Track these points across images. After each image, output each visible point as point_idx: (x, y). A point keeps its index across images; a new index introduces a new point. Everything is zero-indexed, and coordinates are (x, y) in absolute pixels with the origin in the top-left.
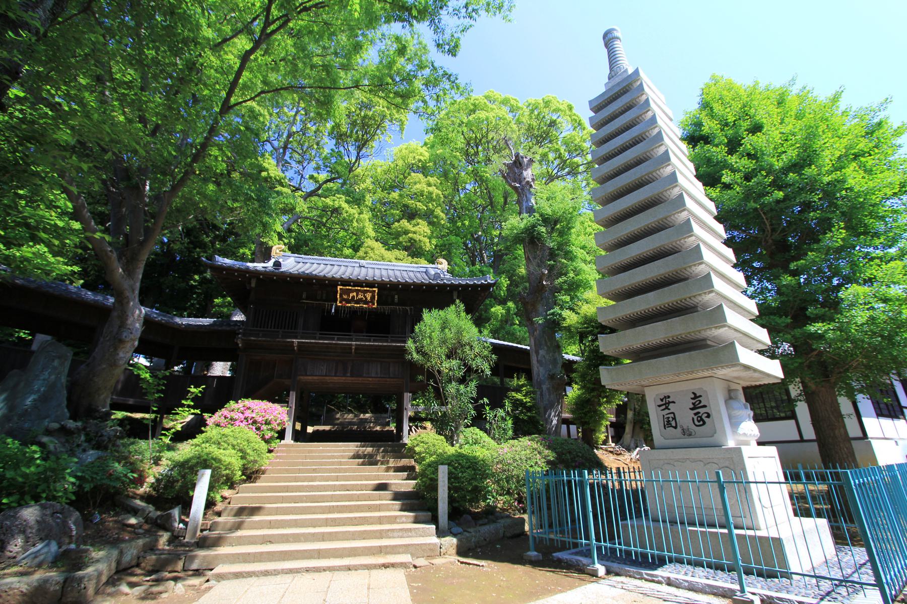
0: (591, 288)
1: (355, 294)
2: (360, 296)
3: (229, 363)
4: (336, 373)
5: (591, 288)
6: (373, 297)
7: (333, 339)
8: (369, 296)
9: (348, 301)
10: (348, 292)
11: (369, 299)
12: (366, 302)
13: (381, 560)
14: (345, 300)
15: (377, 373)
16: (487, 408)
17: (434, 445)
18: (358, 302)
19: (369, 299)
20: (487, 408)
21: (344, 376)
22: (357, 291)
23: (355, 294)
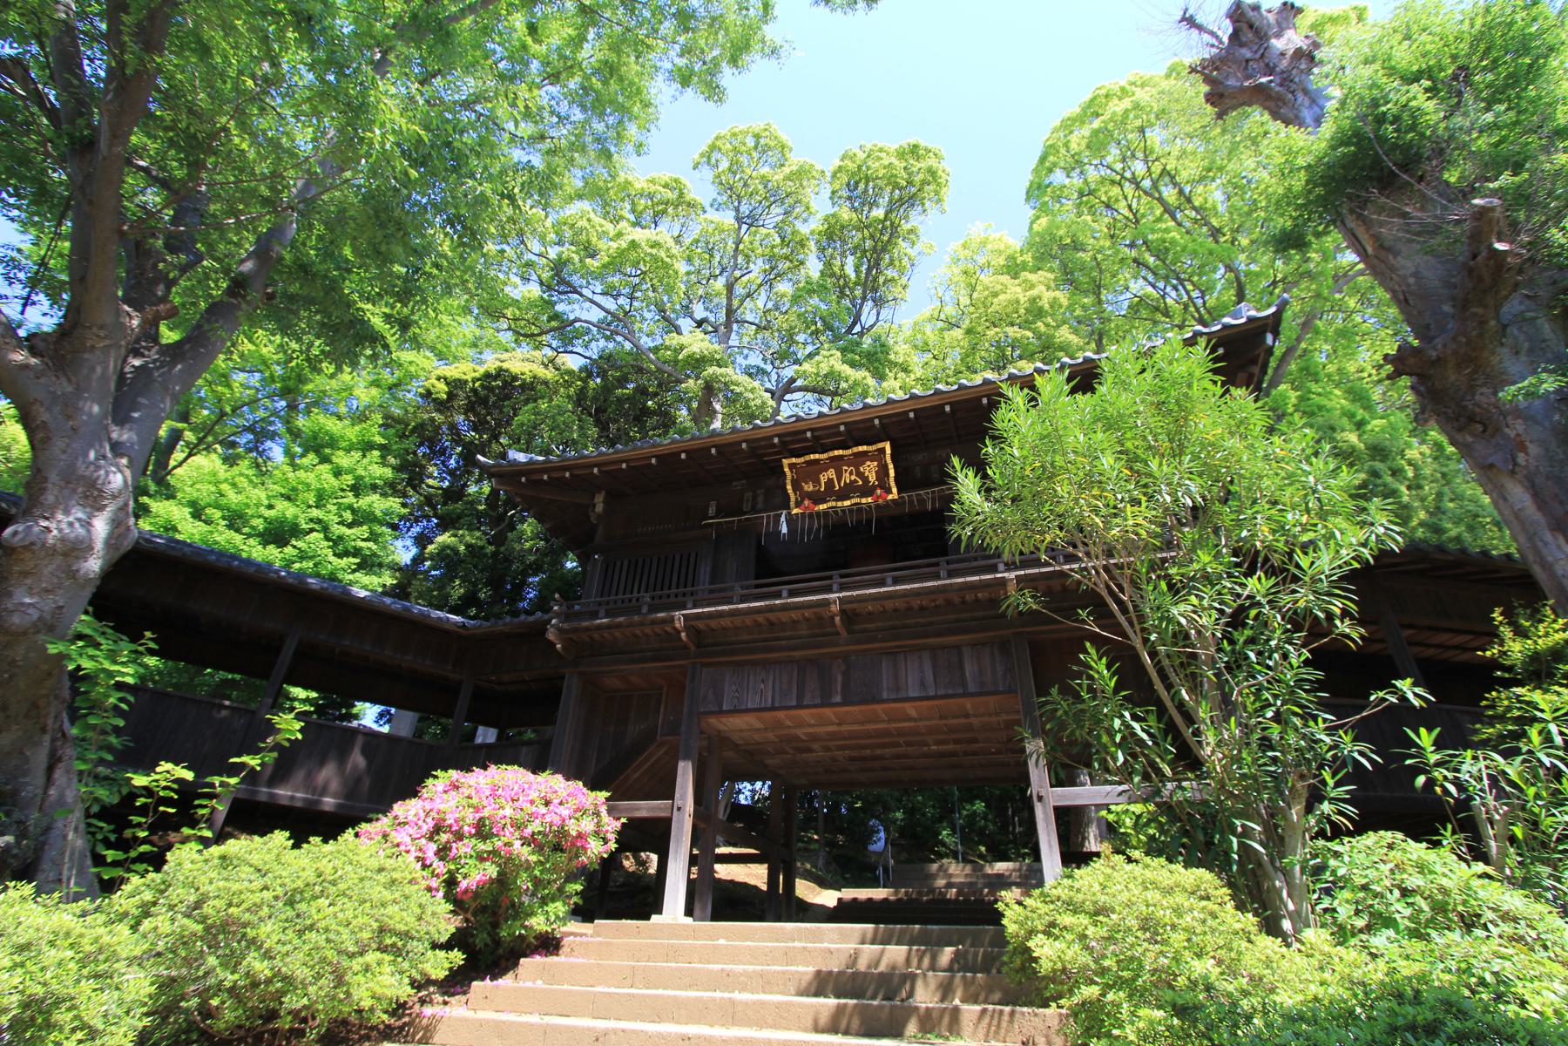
0: (942, 1000)
1: (831, 473)
2: (847, 478)
3: (764, 888)
4: (800, 697)
5: (942, 1000)
6: (882, 472)
7: (778, 595)
8: (870, 470)
9: (818, 498)
10: (815, 468)
11: (872, 478)
12: (867, 490)
13: (792, 642)
14: (810, 496)
15: (923, 685)
16: (1425, 738)
17: (1148, 924)
18: (843, 494)
19: (872, 478)
20: (1425, 738)
21: (826, 703)
22: (837, 462)
23: (831, 473)
